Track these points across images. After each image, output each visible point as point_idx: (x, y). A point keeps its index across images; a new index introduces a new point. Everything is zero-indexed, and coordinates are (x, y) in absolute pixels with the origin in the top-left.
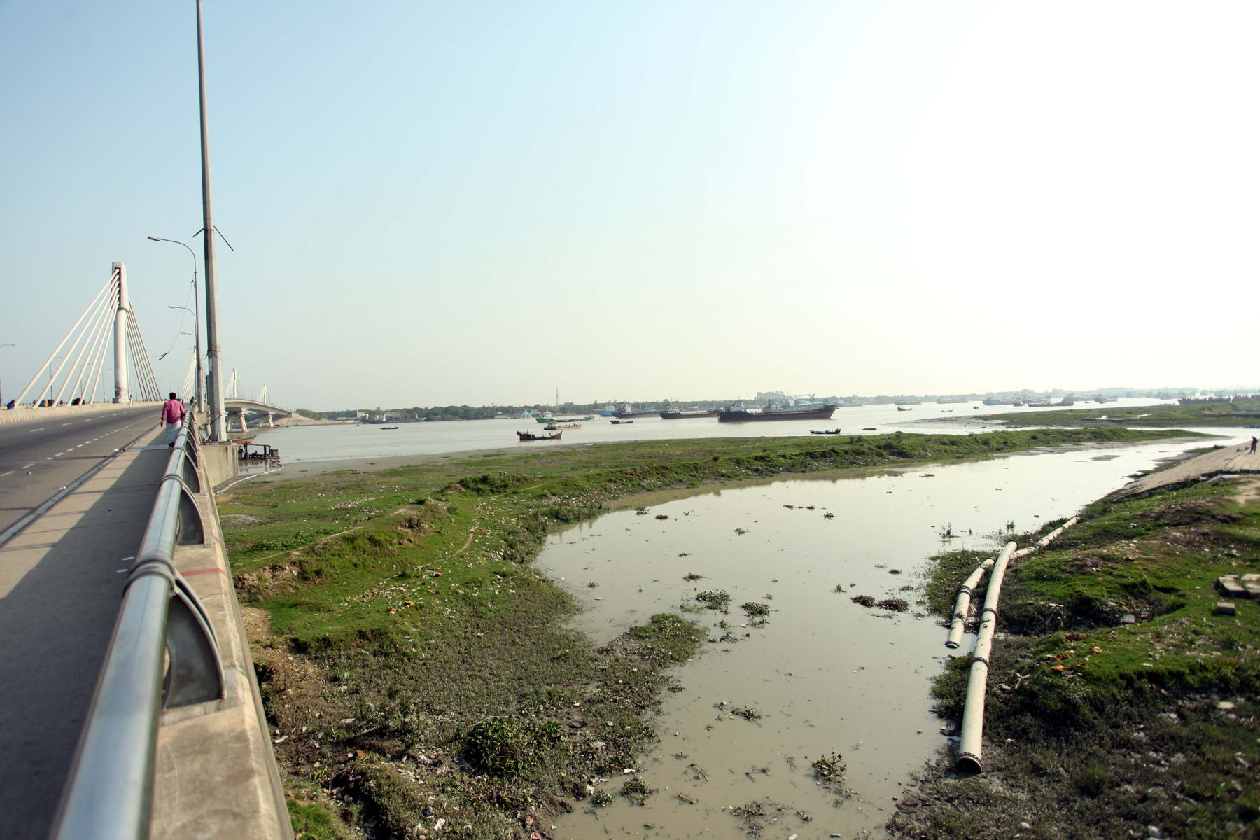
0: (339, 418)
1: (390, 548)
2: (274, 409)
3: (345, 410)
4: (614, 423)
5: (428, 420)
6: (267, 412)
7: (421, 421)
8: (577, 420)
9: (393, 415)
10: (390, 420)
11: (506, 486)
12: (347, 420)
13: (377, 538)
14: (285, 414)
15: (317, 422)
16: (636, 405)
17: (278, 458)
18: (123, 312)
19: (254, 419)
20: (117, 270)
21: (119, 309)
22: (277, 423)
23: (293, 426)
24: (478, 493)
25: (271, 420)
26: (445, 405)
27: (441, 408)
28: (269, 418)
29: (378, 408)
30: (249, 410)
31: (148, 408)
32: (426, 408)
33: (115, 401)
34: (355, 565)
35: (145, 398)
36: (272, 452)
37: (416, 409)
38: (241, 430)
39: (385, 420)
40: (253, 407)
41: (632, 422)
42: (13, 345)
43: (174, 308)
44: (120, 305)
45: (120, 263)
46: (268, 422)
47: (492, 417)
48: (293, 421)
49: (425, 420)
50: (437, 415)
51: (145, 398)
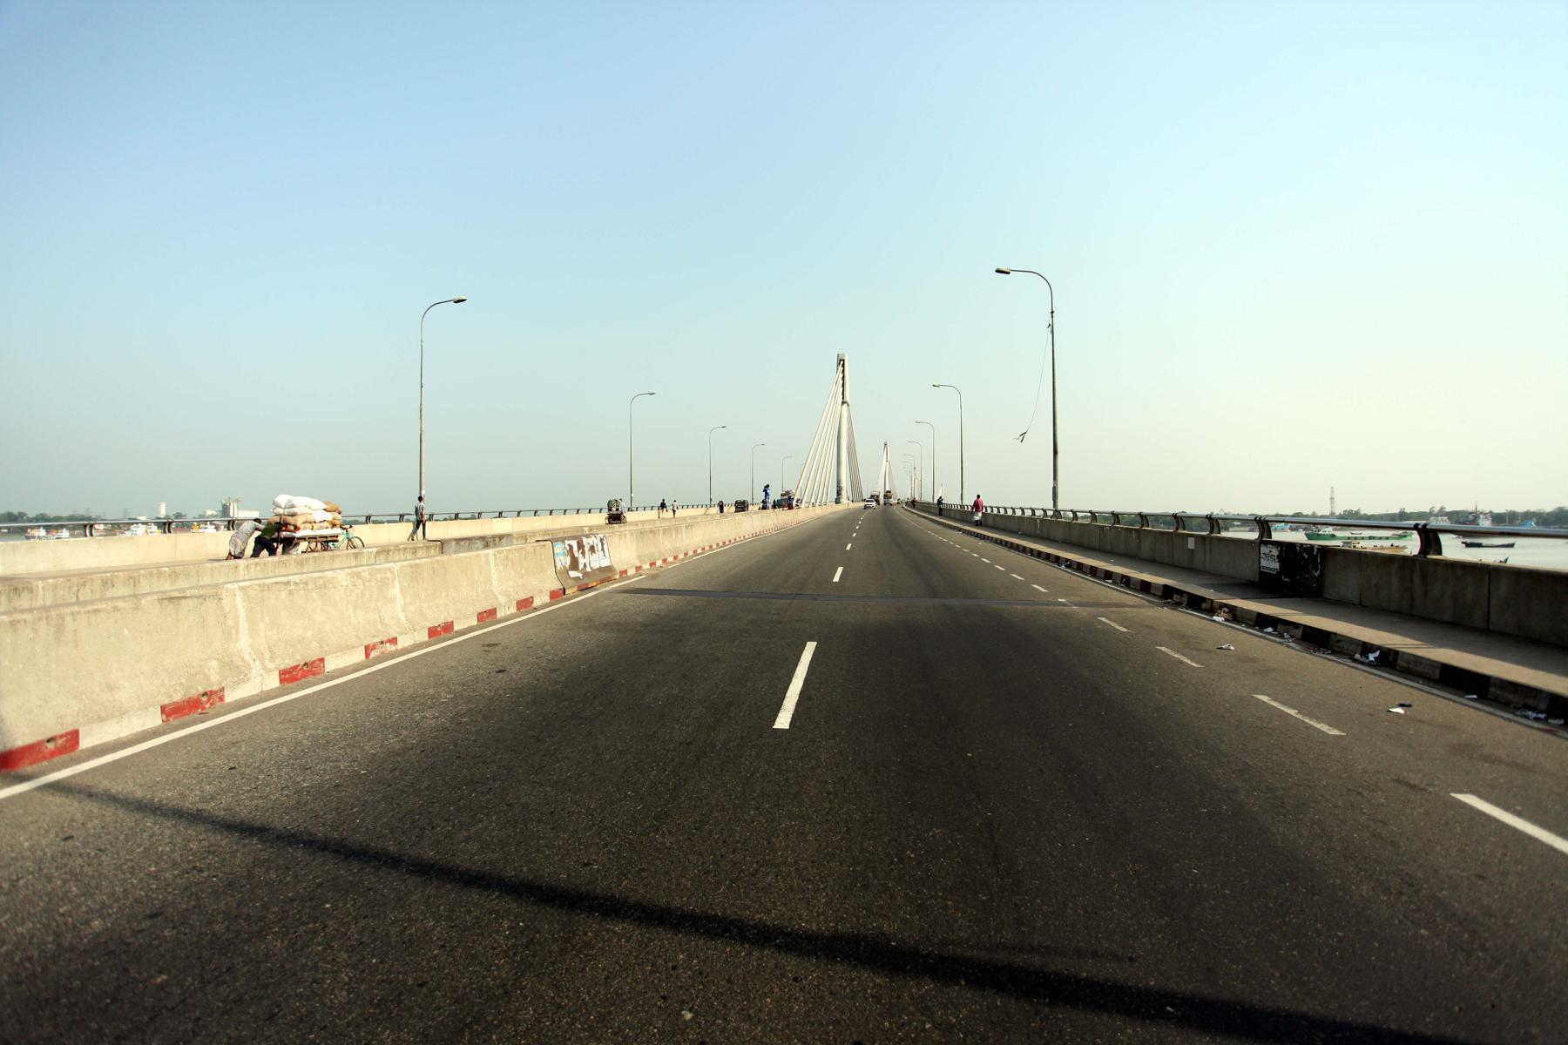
3: (1394, 509)
8: (1380, 538)
16: (1497, 518)
20: (841, 362)
21: (843, 403)
33: (837, 501)
41: (1511, 546)
45: (844, 355)
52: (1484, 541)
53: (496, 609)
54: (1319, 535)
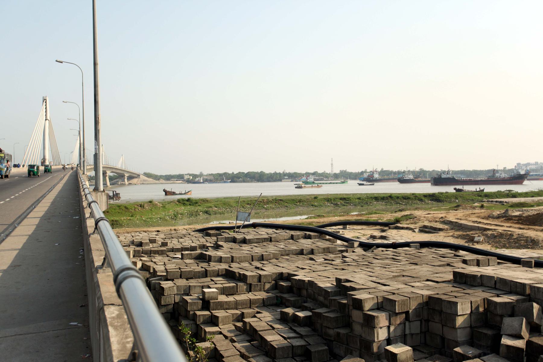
0: (172, 179)
1: (131, 210)
2: (128, 172)
3: (178, 174)
4: (360, 184)
5: (233, 181)
6: (124, 174)
7: (228, 182)
9: (209, 178)
10: (206, 181)
11: (196, 203)
12: (177, 180)
13: (127, 207)
14: (136, 176)
15: (157, 182)
16: (382, 172)
17: (120, 198)
18: (47, 121)
19: (116, 179)
20: (45, 100)
21: (46, 120)
22: (130, 182)
23: (141, 184)
24: (184, 205)
25: (126, 180)
26: (246, 172)
27: (243, 173)
28: (125, 178)
29: (201, 173)
30: (111, 172)
31: (57, 169)
32: (233, 173)
34: (119, 213)
35: (56, 164)
36: (117, 194)
37: (225, 174)
38: (106, 186)
39: (202, 181)
40: (114, 170)
41: (373, 184)
42: (4, 139)
43: (70, 119)
44: (46, 118)
46: (124, 181)
47: (280, 180)
48: (141, 181)
49: (230, 182)
50: (239, 178)
51: (56, 164)
52: (427, 188)
53: (336, 278)
54: (307, 182)
